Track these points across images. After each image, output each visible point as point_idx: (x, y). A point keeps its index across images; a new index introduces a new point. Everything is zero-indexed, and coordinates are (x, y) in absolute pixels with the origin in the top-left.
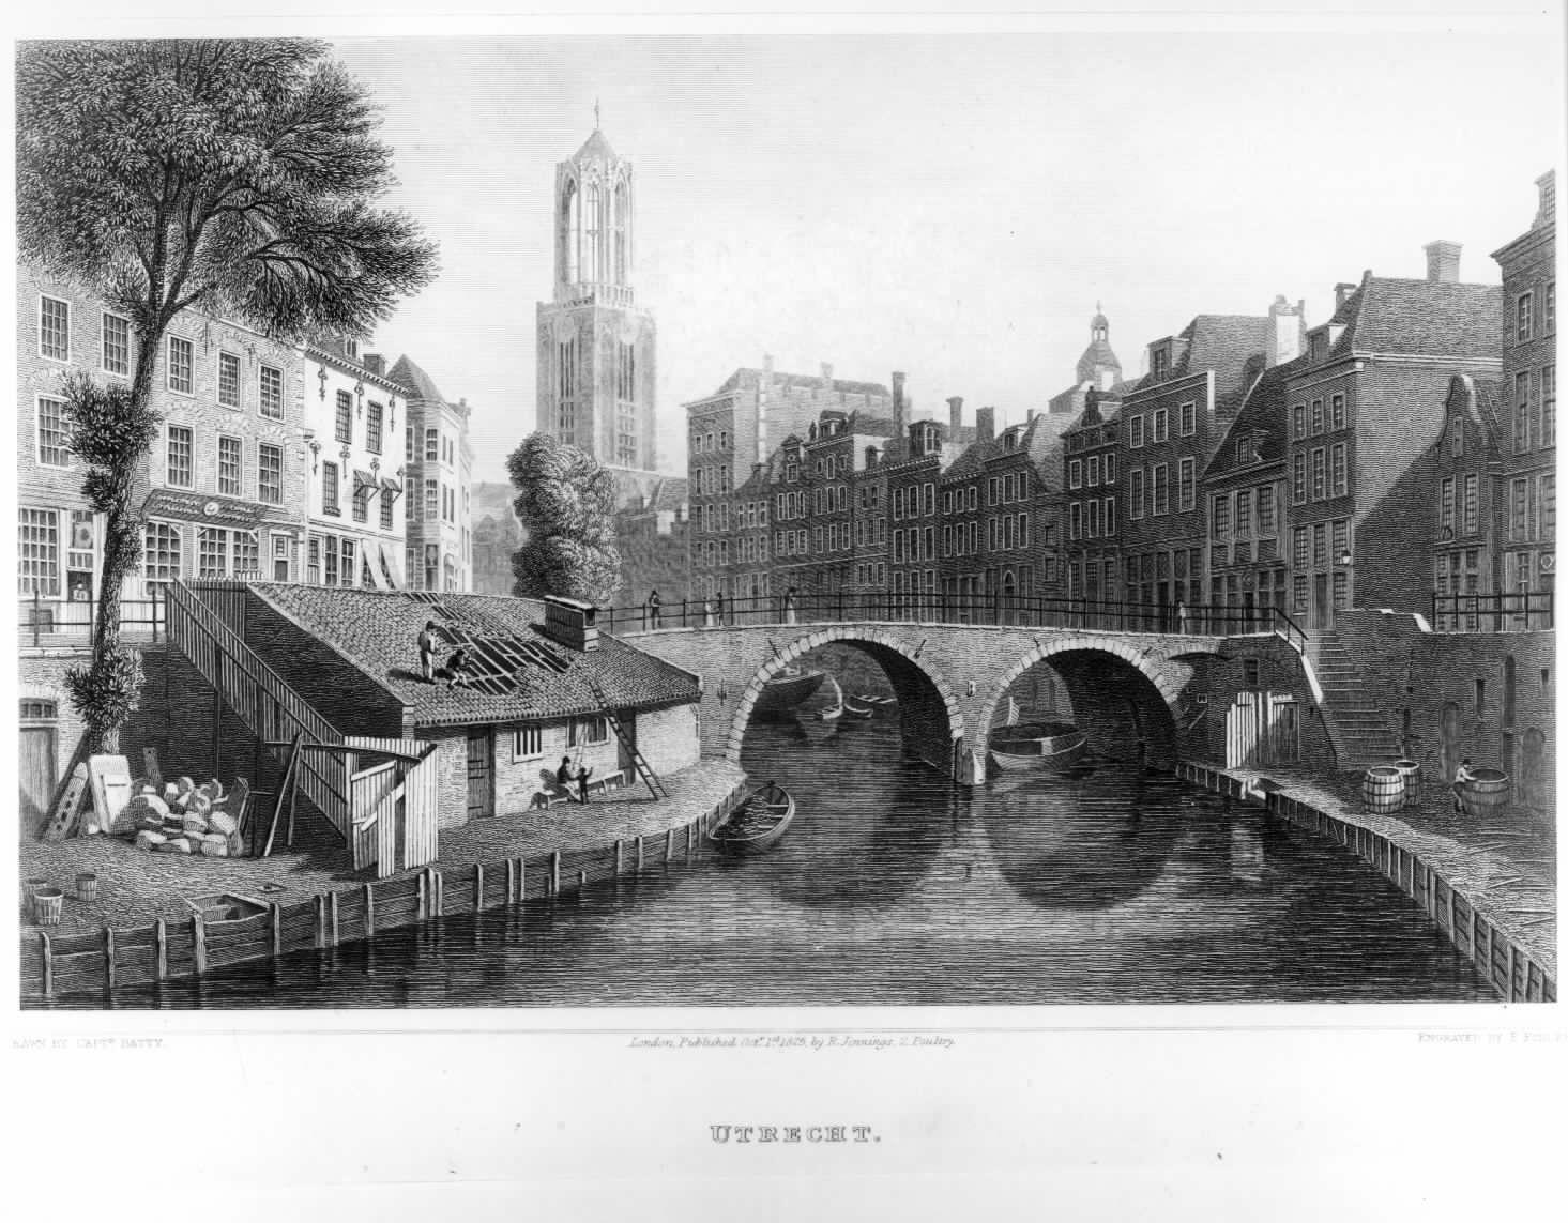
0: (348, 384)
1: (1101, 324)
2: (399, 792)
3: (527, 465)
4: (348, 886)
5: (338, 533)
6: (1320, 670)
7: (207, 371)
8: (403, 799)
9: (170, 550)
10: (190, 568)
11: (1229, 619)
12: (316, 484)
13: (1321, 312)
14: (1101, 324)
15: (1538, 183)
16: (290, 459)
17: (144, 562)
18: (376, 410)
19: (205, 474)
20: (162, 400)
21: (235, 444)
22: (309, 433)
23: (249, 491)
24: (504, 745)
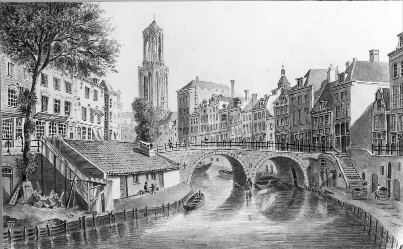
0: (89, 86)
1: (283, 72)
2: (103, 192)
3: (138, 105)
4: (306, 176)
5: (86, 126)
6: (257, 180)
7: (50, 82)
8: (103, 194)
9: (42, 129)
10: (47, 134)
11: (320, 147)
12: (80, 113)
13: (343, 69)
14: (283, 72)
15: (398, 36)
16: (73, 107)
17: (36, 133)
18: (96, 92)
19: (51, 110)
20: (39, 89)
21: (59, 102)
22: (79, 98)
23: (62, 113)
24: (130, 180)
